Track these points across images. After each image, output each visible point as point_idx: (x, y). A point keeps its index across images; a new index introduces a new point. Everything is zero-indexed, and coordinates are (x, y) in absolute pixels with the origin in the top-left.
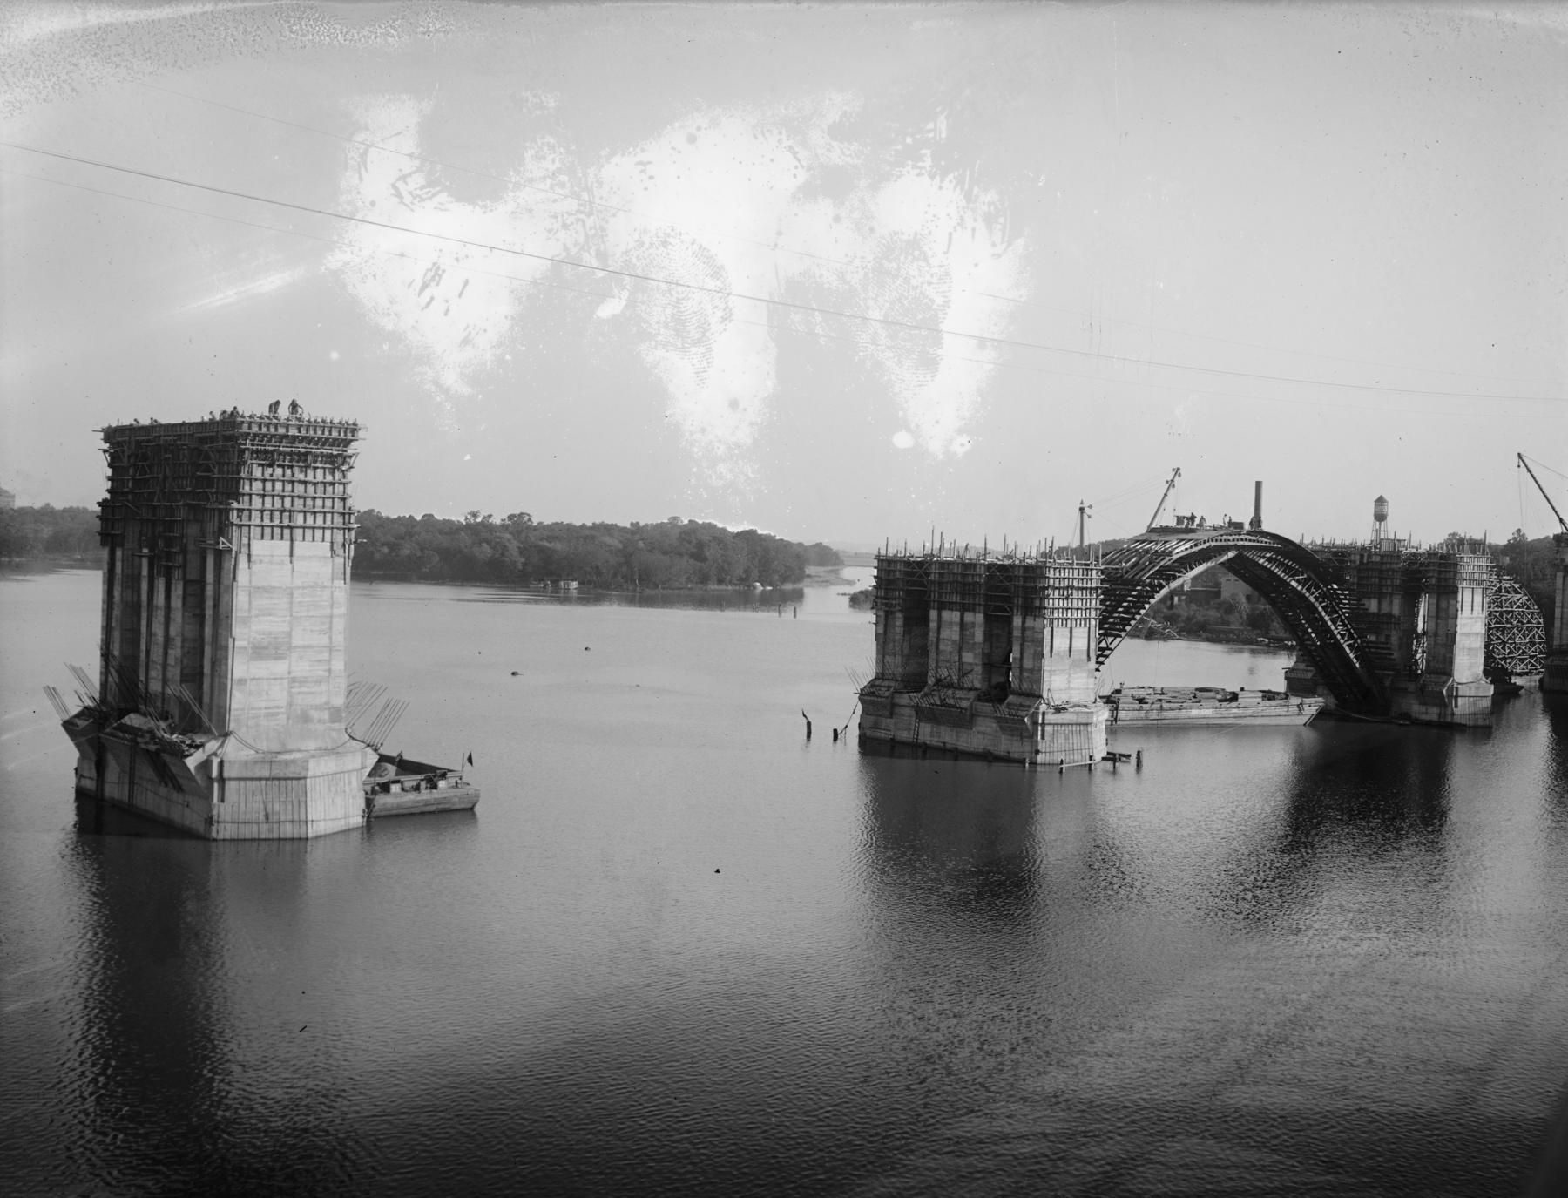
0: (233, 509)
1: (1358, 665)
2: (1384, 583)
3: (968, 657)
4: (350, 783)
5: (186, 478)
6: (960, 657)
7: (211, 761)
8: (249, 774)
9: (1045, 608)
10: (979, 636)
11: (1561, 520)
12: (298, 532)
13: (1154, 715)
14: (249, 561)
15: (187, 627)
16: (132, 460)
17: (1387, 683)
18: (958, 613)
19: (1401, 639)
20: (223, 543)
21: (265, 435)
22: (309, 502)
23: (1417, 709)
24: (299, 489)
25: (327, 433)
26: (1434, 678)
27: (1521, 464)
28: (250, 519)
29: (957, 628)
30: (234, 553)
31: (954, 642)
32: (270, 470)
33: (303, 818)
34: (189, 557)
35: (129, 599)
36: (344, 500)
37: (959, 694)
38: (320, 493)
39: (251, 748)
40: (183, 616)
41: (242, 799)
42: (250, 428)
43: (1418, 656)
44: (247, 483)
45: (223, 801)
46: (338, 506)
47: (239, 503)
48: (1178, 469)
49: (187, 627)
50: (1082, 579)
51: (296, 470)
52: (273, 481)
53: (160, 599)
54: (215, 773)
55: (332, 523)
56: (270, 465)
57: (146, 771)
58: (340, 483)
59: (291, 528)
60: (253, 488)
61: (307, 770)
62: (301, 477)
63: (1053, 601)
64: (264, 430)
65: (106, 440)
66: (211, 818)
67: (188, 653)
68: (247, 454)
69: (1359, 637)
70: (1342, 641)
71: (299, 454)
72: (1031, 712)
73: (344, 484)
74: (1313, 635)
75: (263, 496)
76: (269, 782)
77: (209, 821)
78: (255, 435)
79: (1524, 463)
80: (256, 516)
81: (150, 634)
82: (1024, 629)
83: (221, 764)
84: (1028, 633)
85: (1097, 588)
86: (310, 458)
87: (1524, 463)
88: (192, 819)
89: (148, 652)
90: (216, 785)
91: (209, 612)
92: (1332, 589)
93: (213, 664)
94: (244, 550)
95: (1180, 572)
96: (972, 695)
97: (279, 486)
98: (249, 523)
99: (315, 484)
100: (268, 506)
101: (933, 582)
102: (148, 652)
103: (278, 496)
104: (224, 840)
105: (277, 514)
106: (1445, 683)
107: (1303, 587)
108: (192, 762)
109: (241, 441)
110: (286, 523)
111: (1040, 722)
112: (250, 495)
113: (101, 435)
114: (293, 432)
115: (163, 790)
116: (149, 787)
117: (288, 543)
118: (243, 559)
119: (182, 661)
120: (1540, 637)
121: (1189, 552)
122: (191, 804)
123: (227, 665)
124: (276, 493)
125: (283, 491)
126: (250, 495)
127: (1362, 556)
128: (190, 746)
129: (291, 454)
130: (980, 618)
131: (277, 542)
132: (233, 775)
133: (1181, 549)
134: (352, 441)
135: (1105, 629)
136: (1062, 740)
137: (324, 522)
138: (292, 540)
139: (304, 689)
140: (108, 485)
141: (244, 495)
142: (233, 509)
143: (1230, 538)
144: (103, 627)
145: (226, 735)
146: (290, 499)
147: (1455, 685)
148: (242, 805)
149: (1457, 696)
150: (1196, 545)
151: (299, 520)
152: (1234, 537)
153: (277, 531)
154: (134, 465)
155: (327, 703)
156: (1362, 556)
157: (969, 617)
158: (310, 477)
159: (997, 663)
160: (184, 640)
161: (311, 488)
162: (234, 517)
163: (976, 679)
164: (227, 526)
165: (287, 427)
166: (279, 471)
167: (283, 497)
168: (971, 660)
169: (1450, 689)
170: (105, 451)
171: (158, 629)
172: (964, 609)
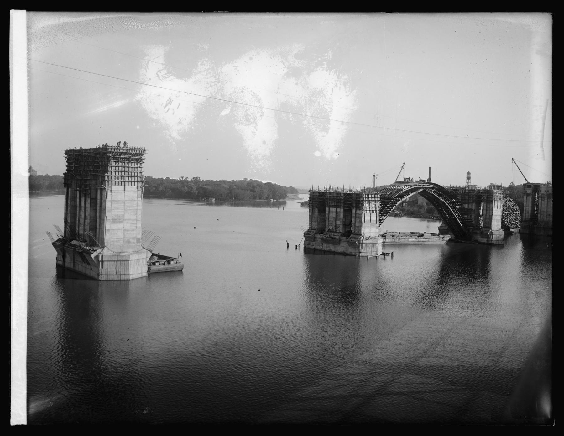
0: (106, 176)
1: (461, 225)
3: (338, 222)
4: (143, 262)
6: (336, 222)
7: (99, 255)
8: (111, 260)
9: (363, 207)
10: (342, 215)
11: (526, 179)
12: (127, 183)
13: (397, 241)
14: (111, 192)
15: (92, 213)
17: (471, 231)
18: (335, 209)
19: (475, 217)
20: (103, 186)
22: (130, 173)
24: (127, 169)
25: (136, 152)
27: (513, 161)
29: (335, 213)
31: (334, 218)
32: (118, 163)
33: (128, 273)
35: (73, 204)
37: (336, 234)
40: (90, 209)
41: (109, 267)
42: (111, 150)
44: (110, 167)
45: (103, 268)
46: (139, 175)
47: (108, 174)
48: (405, 163)
49: (92, 213)
50: (374, 198)
51: (126, 163)
54: (100, 259)
57: (78, 259)
58: (140, 168)
59: (124, 182)
60: (112, 169)
61: (129, 258)
62: (128, 165)
64: (116, 151)
67: (92, 221)
69: (462, 216)
70: (456, 217)
73: (141, 168)
76: (117, 262)
77: (98, 274)
79: (514, 161)
81: (80, 215)
82: (356, 214)
83: (102, 256)
84: (357, 215)
85: (379, 201)
86: (130, 160)
87: (514, 161)
88: (93, 274)
90: (100, 263)
92: (453, 201)
93: (100, 225)
94: (110, 189)
96: (339, 234)
99: (132, 168)
100: (117, 175)
106: (489, 231)
107: (444, 200)
108: (93, 256)
110: (123, 180)
111: (361, 243)
112: (111, 171)
113: (64, 152)
114: (125, 151)
115: (84, 265)
116: (79, 263)
117: (123, 186)
119: (90, 224)
120: (519, 216)
121: (408, 189)
122: (93, 269)
123: (104, 225)
124: (119, 171)
126: (111, 171)
127: (463, 191)
128: (92, 251)
129: (124, 158)
130: (342, 210)
131: (120, 186)
132: (106, 260)
133: (405, 188)
134: (143, 154)
136: (368, 249)
137: (135, 180)
138: (124, 185)
139: (128, 233)
141: (109, 171)
142: (106, 176)
143: (421, 185)
145: (104, 247)
146: (117, 177)
147: (492, 231)
148: (109, 269)
150: (410, 187)
151: (127, 179)
152: (422, 184)
153: (120, 183)
155: (136, 237)
156: (463, 191)
157: (338, 210)
158: (130, 166)
160: (90, 217)
161: (130, 169)
162: (106, 178)
163: (341, 229)
165: (123, 150)
166: (120, 164)
168: (339, 224)
169: (491, 233)
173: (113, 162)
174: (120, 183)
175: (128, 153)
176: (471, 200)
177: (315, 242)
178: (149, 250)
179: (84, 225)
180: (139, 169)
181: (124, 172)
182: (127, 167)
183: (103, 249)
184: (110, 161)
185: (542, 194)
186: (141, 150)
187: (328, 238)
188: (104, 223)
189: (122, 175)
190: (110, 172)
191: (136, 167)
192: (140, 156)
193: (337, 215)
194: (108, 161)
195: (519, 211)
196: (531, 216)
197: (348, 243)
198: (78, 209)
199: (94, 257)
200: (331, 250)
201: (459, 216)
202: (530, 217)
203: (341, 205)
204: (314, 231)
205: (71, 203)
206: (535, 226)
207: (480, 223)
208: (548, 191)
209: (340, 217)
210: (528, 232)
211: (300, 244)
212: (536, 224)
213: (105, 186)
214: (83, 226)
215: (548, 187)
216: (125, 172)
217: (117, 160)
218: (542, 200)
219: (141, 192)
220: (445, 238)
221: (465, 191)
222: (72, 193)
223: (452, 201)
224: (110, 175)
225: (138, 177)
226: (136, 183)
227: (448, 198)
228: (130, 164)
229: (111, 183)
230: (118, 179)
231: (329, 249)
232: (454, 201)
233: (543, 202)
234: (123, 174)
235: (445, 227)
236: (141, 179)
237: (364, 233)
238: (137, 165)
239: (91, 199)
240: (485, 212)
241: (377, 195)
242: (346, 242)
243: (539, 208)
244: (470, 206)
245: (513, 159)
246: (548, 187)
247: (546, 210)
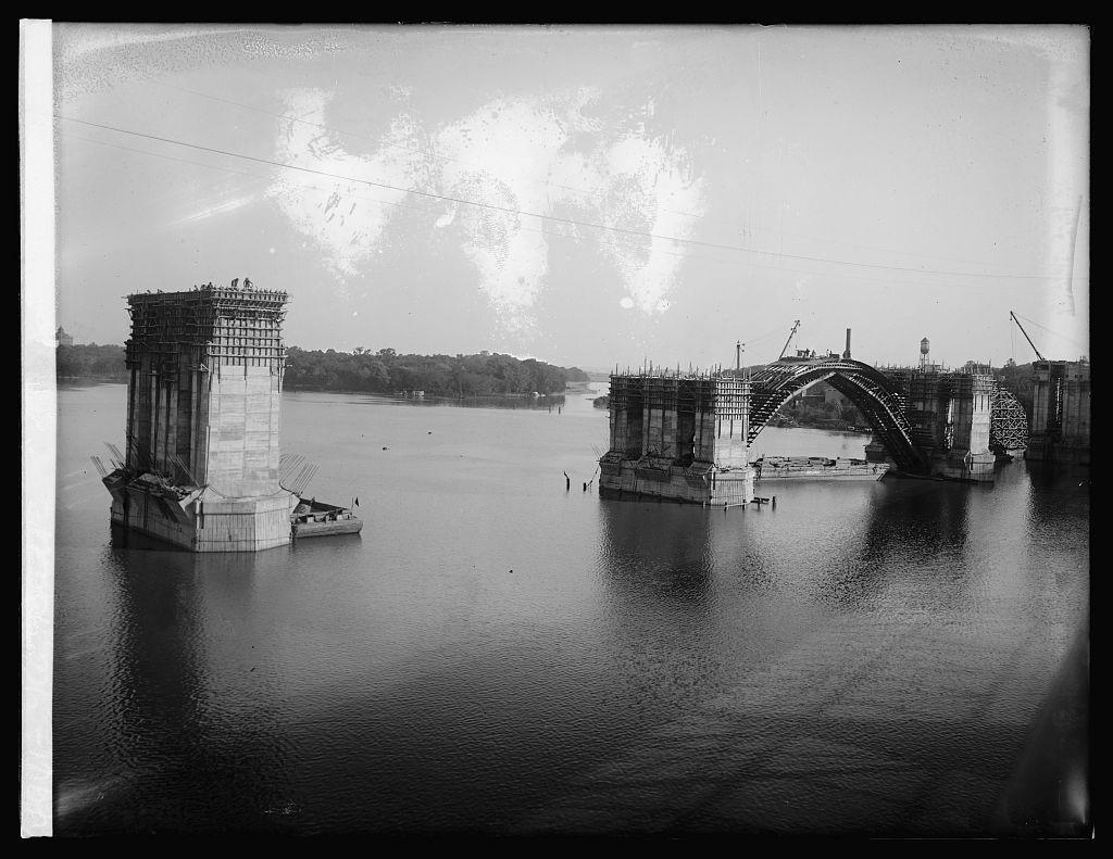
3: (667, 438)
10: (674, 425)
22: (257, 342)
23: (948, 471)
24: (250, 334)
37: (662, 461)
51: (248, 322)
53: (163, 402)
54: (198, 511)
57: (156, 510)
63: (721, 403)
64: (228, 297)
68: (218, 312)
77: (194, 541)
88: (184, 539)
93: (196, 443)
94: (216, 372)
97: (237, 331)
108: (183, 504)
115: (165, 521)
118: (215, 377)
128: (182, 494)
129: (245, 312)
130: (675, 414)
133: (800, 371)
145: (205, 487)
157: (668, 413)
158: (257, 327)
159: (685, 443)
161: (258, 333)
163: (673, 452)
166: (238, 322)
167: (240, 339)
186: (277, 295)
201: (906, 426)
202: (1045, 427)
226: (268, 361)
228: (257, 323)
233: (1072, 398)
239: (180, 392)
243: (1064, 410)
244: (927, 406)
247: (1077, 414)
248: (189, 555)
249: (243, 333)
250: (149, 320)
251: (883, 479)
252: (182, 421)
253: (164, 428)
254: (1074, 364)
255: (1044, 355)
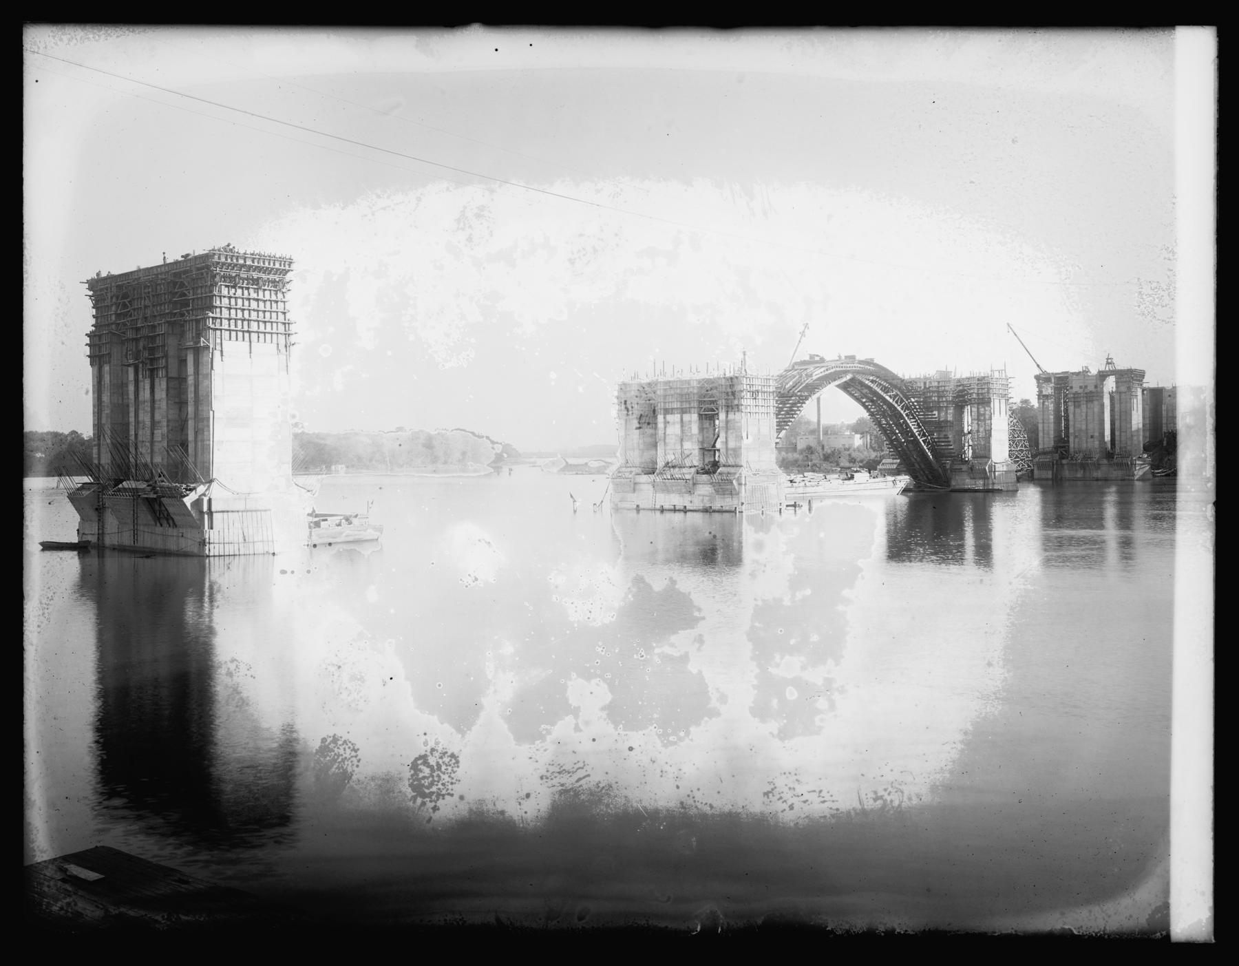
0: (209, 318)
2: (941, 400)
3: (688, 445)
5: (165, 304)
6: (682, 445)
7: (203, 499)
9: (742, 405)
10: (695, 429)
11: (1038, 366)
12: (254, 336)
13: (801, 490)
14: (222, 355)
15: (171, 412)
16: (114, 300)
17: (948, 467)
18: (679, 416)
19: (954, 436)
20: (204, 342)
21: (230, 265)
22: (261, 314)
23: (968, 483)
24: (254, 305)
25: (272, 264)
26: (980, 460)
27: (1010, 330)
28: (221, 325)
29: (678, 426)
30: (211, 349)
31: (677, 435)
32: (233, 290)
33: (270, 539)
34: (169, 360)
35: (116, 401)
36: (284, 313)
37: (684, 470)
38: (268, 308)
39: (229, 490)
40: (167, 403)
41: (226, 527)
42: (219, 258)
43: (966, 448)
44: (218, 298)
45: (212, 528)
46: (281, 317)
47: (213, 313)
48: (807, 324)
49: (171, 412)
50: (764, 386)
51: (251, 291)
52: (236, 298)
53: (145, 394)
54: (205, 508)
55: (277, 330)
56: (234, 287)
57: (145, 516)
58: (282, 302)
59: (249, 332)
60: (223, 303)
62: (255, 296)
63: (747, 401)
64: (229, 261)
65: (90, 289)
66: (204, 540)
67: (172, 430)
68: (217, 279)
69: (929, 435)
70: (919, 437)
71: (253, 279)
72: (736, 477)
73: (284, 302)
74: (899, 435)
75: (230, 309)
76: (245, 514)
77: (203, 543)
78: (224, 264)
79: (1011, 328)
80: (225, 322)
81: (137, 422)
82: (727, 422)
83: (210, 501)
85: (773, 392)
86: (261, 283)
87: (1011, 328)
88: (188, 545)
89: (136, 435)
90: (206, 516)
91: (191, 396)
92: (911, 402)
93: (196, 433)
94: (218, 347)
95: (818, 389)
96: (693, 470)
97: (240, 301)
98: (220, 328)
99: (265, 301)
100: (233, 316)
101: (659, 396)
102: (136, 435)
103: (240, 309)
104: (214, 556)
105: (239, 323)
106: (986, 463)
107: (894, 400)
108: (188, 501)
109: (212, 268)
110: (246, 328)
111: (744, 483)
112: (221, 308)
113: (87, 286)
114: (249, 262)
115: (159, 529)
116: (146, 530)
117: (248, 343)
118: (217, 354)
119: (167, 436)
120: (1026, 447)
121: (823, 374)
122: (184, 535)
123: (209, 431)
124: (238, 307)
125: (243, 306)
126: (221, 308)
127: (925, 383)
128: (187, 490)
129: (247, 279)
130: (695, 417)
131: (240, 343)
133: (818, 373)
134: (289, 271)
135: (780, 418)
137: (272, 329)
138: (250, 342)
140: (93, 321)
141: (216, 307)
142: (209, 318)
143: (848, 365)
144: (94, 425)
145: (211, 481)
146: (234, 321)
147: (993, 464)
148: (226, 530)
149: (995, 471)
150: (827, 370)
151: (254, 326)
152: (850, 365)
153: (240, 334)
154: (116, 304)
156: (925, 383)
157: (686, 417)
158: (261, 296)
159: (708, 449)
160: (168, 421)
161: (261, 304)
162: (210, 323)
163: (696, 460)
164: (205, 330)
165: (245, 259)
166: (239, 292)
167: (243, 310)
169: (990, 467)
170: (90, 296)
171: (145, 417)
172: (683, 411)
173: (223, 287)
174: (240, 334)
175: (257, 267)
176: (943, 402)
177: (635, 495)
178: (309, 491)
179: (152, 442)
180: (281, 305)
181: (247, 309)
182: (254, 299)
183: (209, 487)
184: (216, 284)
185: (1074, 394)
186: (282, 260)
187: (667, 481)
188: (209, 426)
189: (243, 316)
190: (218, 310)
191: (274, 301)
192: (281, 276)
193: (684, 428)
194: (212, 285)
195: (1026, 436)
196: (1055, 441)
197: (714, 486)
198: (132, 409)
199: (191, 504)
200: (674, 506)
201: (924, 435)
202: (1052, 444)
203: (692, 405)
204: (633, 469)
205: (110, 399)
206: (1064, 462)
207: (965, 451)
208: (1086, 387)
209: (691, 432)
210: (1051, 477)
211: (602, 502)
212: (1067, 458)
213: (209, 343)
214: (148, 444)
215: (1086, 378)
216: (249, 310)
217: (233, 282)
218: (1075, 407)
219: (285, 357)
220: (898, 482)
221: (930, 382)
222: (112, 375)
223: (909, 403)
224: (218, 315)
225: (279, 324)
226: (275, 336)
227: (901, 396)
228: (261, 293)
229: (221, 336)
230: (236, 326)
231: (670, 505)
232: (913, 403)
233: (1078, 410)
234: (246, 316)
235: (893, 463)
236: (285, 327)
237: (747, 462)
238: (276, 294)
239: (169, 379)
240: (975, 427)
241: (769, 379)
242: (709, 486)
243: (1071, 423)
244: (943, 414)
245: (1008, 324)
246: (1086, 378)
247: (1084, 427)
248: (195, 560)
249: (246, 303)
250: (118, 305)
251: (905, 491)
252: (173, 414)
253: (148, 423)
254: (1078, 374)
255: (1045, 368)
